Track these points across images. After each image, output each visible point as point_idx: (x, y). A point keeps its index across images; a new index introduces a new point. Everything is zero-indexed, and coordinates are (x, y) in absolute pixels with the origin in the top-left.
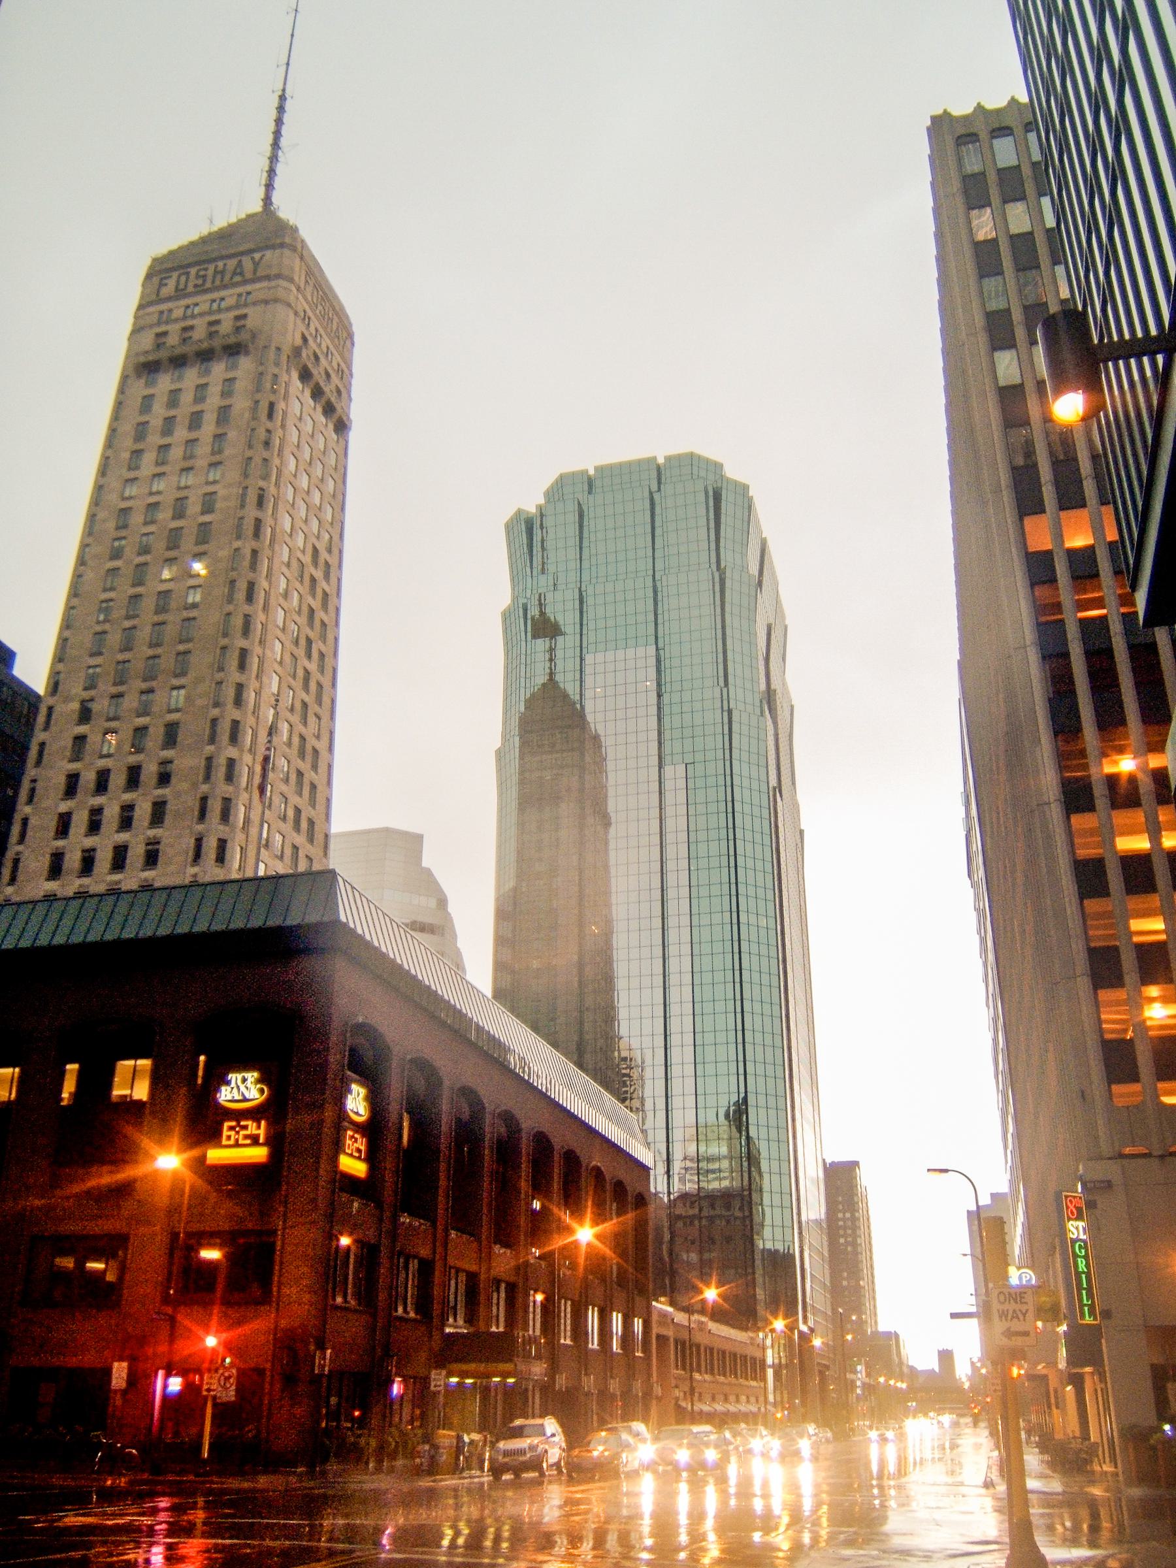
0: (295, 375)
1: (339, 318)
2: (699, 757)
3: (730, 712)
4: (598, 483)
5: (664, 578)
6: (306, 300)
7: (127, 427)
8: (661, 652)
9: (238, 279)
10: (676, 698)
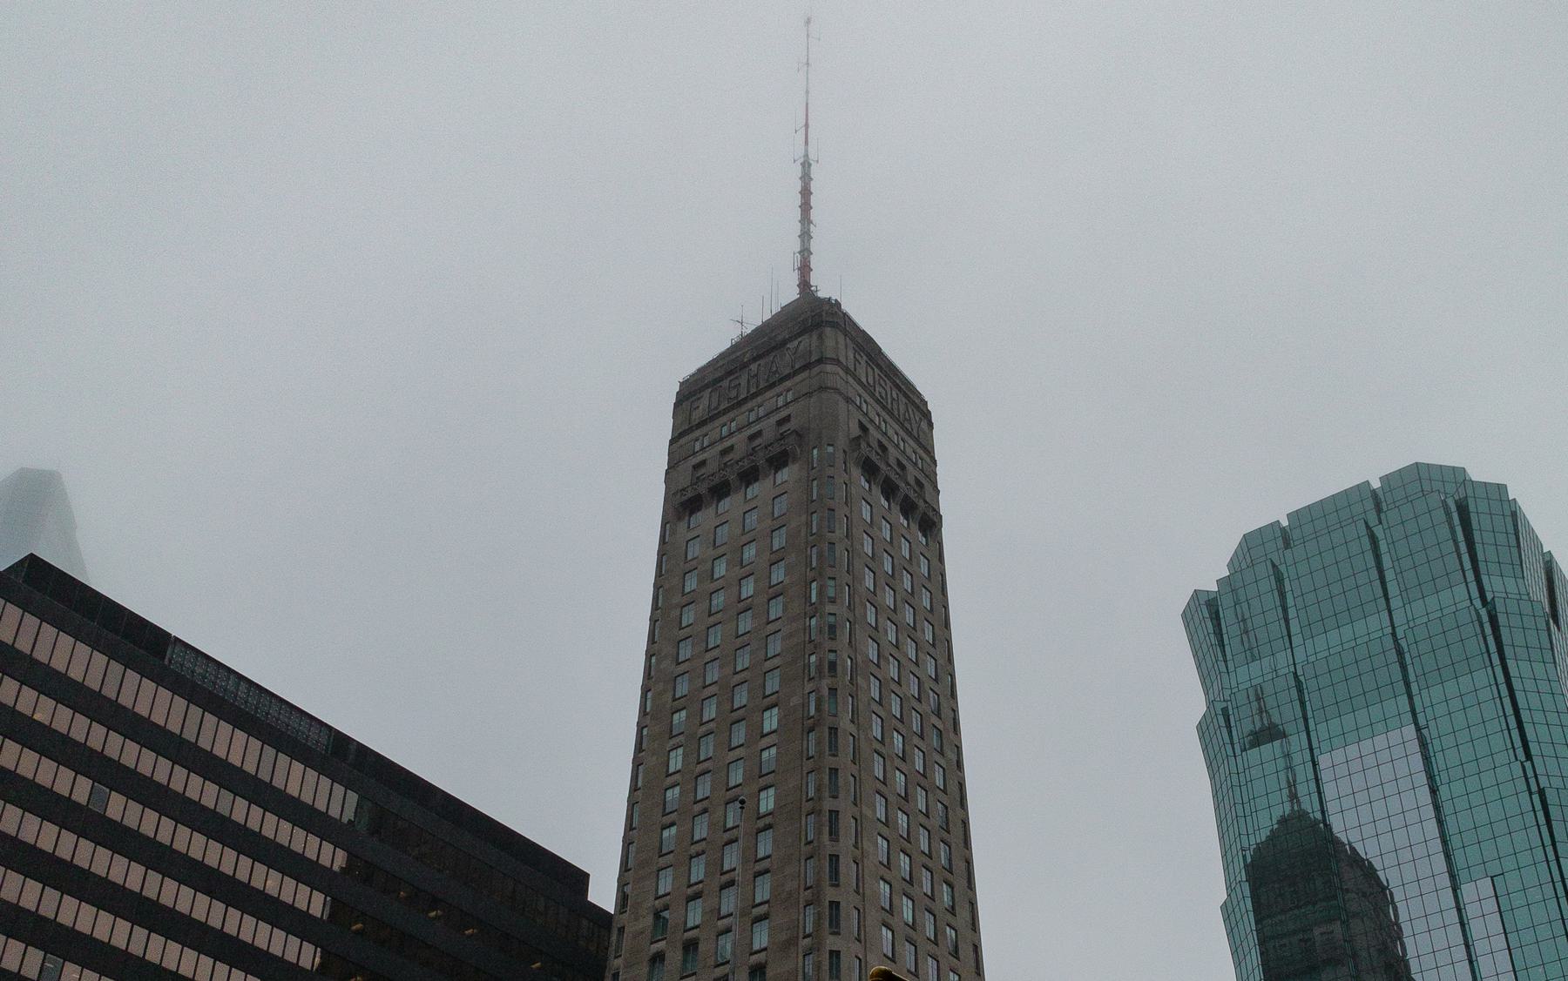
0: (856, 472)
2: (1509, 864)
3: (1541, 792)
4: (1296, 535)
5: (1409, 633)
6: (859, 382)
8: (1425, 732)
10: (1458, 788)
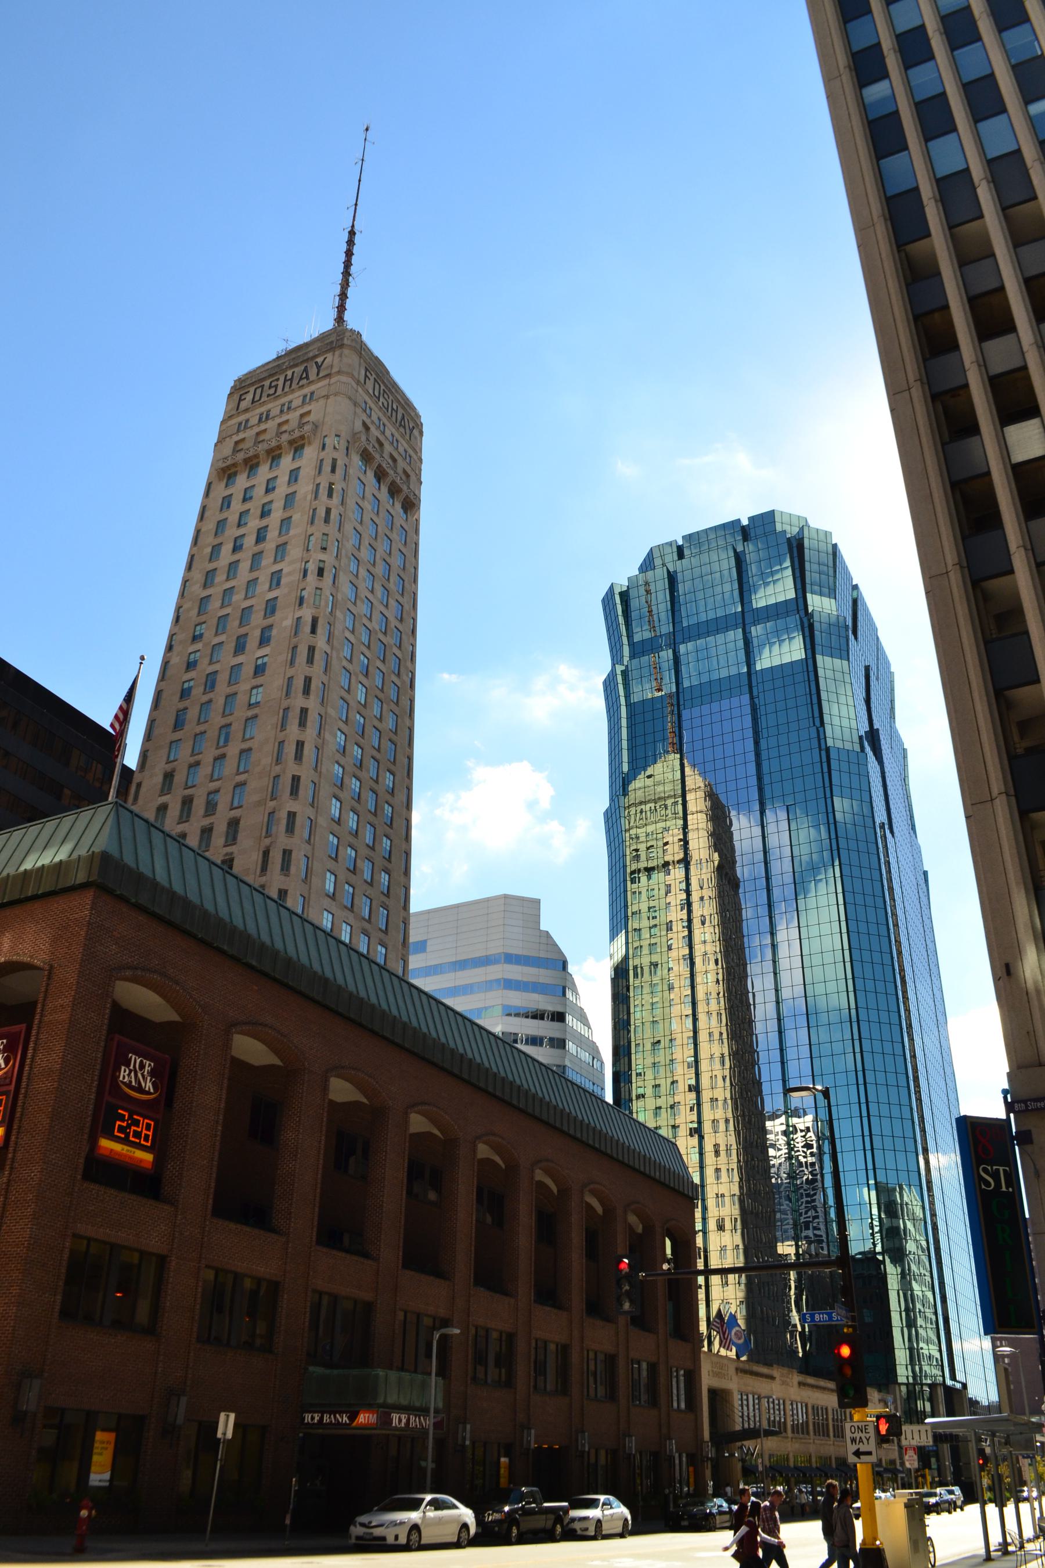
1: (403, 408)
7: (210, 526)
8: (756, 700)
9: (304, 381)
10: (773, 742)
